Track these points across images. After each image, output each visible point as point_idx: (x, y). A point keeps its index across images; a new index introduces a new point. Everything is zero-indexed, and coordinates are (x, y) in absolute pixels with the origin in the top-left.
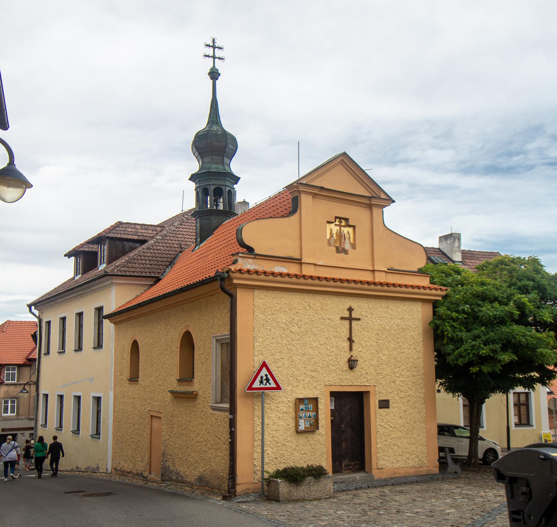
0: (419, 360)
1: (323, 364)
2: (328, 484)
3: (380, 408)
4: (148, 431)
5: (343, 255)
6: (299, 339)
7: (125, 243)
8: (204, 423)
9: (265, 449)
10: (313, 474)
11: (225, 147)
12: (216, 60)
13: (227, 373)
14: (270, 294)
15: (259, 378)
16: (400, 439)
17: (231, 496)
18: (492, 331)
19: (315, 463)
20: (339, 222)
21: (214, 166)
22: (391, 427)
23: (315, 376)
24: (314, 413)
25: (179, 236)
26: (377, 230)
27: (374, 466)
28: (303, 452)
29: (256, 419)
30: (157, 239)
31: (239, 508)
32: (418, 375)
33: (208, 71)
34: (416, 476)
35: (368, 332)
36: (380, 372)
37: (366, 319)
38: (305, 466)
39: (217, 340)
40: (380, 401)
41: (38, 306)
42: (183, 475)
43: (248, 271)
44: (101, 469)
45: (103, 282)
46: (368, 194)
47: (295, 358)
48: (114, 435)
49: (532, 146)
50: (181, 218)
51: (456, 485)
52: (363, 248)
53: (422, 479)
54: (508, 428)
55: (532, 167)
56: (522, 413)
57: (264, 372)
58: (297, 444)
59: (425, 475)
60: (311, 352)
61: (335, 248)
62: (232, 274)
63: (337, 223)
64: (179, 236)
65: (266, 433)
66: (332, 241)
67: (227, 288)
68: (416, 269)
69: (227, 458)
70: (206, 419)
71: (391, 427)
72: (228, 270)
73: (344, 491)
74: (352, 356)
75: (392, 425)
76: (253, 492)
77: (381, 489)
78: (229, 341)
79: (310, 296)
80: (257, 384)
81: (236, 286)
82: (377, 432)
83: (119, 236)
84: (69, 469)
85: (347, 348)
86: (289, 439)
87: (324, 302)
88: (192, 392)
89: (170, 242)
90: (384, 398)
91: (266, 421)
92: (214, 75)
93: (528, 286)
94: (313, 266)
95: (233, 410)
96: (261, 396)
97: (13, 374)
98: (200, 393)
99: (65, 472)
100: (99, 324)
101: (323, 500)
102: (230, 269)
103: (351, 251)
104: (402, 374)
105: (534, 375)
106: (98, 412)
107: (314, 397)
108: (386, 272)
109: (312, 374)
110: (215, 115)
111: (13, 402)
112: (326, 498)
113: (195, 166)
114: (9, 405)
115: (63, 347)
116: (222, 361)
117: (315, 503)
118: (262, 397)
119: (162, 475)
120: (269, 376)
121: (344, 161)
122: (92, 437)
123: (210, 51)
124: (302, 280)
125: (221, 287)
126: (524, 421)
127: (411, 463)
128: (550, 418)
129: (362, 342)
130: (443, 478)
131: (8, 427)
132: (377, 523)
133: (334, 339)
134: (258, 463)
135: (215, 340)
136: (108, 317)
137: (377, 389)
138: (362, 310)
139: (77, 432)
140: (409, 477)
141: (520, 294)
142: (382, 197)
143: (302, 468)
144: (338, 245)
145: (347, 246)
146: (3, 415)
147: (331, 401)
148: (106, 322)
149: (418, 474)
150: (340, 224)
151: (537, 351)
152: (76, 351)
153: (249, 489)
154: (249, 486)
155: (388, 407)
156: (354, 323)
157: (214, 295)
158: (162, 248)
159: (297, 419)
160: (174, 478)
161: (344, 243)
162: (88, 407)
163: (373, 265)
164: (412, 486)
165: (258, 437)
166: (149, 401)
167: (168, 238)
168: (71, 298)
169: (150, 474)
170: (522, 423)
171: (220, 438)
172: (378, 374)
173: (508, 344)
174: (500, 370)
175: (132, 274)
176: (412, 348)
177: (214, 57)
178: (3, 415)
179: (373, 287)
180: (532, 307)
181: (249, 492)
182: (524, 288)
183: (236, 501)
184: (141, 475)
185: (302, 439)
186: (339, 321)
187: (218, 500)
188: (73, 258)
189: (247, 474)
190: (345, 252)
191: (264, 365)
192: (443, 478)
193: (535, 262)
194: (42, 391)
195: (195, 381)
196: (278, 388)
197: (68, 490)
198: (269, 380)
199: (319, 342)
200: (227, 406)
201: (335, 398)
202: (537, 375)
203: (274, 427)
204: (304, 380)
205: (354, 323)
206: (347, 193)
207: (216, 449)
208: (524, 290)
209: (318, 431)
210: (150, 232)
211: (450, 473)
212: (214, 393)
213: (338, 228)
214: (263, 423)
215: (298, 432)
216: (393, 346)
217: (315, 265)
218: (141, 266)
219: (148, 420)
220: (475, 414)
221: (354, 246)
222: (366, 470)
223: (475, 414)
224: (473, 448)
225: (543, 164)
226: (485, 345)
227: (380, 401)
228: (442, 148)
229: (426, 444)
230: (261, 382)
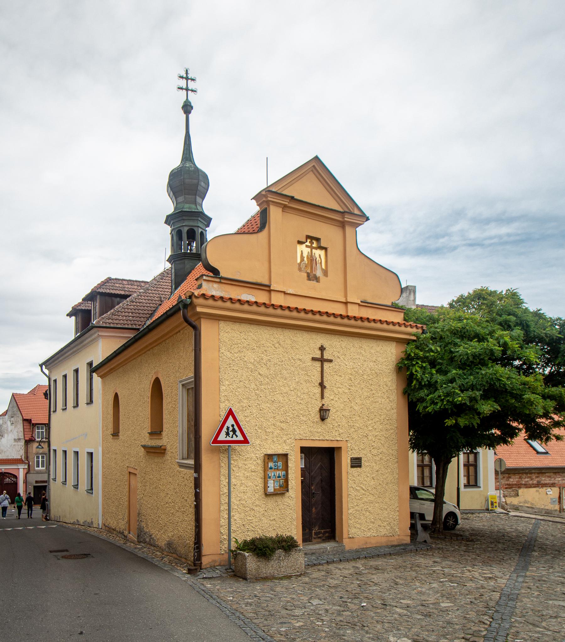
0: (393, 411)
1: (293, 414)
2: (298, 559)
3: (352, 467)
4: (127, 487)
6: (268, 384)
7: (114, 298)
8: (172, 482)
9: (232, 514)
10: (283, 546)
11: (197, 185)
12: (189, 92)
13: (193, 423)
14: (237, 326)
16: (374, 503)
17: (196, 569)
18: (471, 374)
19: (285, 533)
20: (310, 242)
21: (187, 206)
22: (363, 490)
23: (284, 428)
24: (284, 473)
25: (159, 289)
26: (350, 256)
27: (345, 535)
28: (271, 519)
29: (222, 478)
30: (140, 293)
31: (202, 587)
32: (391, 429)
34: (387, 547)
35: (340, 376)
36: (352, 424)
37: (339, 360)
38: (274, 535)
39: (183, 385)
40: (352, 459)
42: (155, 538)
43: (213, 297)
46: (342, 210)
47: (263, 406)
49: (456, 228)
50: (162, 275)
51: (433, 560)
52: (335, 275)
53: (395, 550)
54: (458, 489)
55: (455, 248)
56: (470, 474)
58: (266, 509)
59: (396, 546)
60: (281, 399)
61: (306, 274)
62: (195, 300)
63: (308, 243)
64: (159, 289)
65: (233, 495)
66: (303, 266)
67: (192, 320)
68: (389, 304)
69: (193, 523)
70: (174, 477)
71: (363, 490)
72: (190, 294)
73: (315, 565)
74: (323, 405)
75: (364, 487)
76: (220, 565)
77: (353, 564)
78: (193, 386)
79: (280, 330)
80: (222, 437)
81: (200, 316)
82: (348, 495)
83: (108, 291)
85: (318, 395)
86: (257, 502)
87: (295, 339)
88: (161, 446)
89: (152, 295)
90: (356, 456)
91: (233, 481)
92: (187, 108)
93: (510, 321)
94: (283, 294)
95: (197, 468)
96: (227, 450)
98: (168, 448)
99: (70, 525)
101: (293, 579)
102: (193, 293)
104: (375, 427)
105: (495, 433)
107: (283, 453)
108: (359, 305)
109: (282, 425)
110: (188, 152)
111: (43, 457)
112: (297, 575)
113: (169, 207)
114: (40, 460)
116: (188, 409)
117: (285, 582)
118: (228, 452)
119: (138, 536)
120: (236, 427)
121: (316, 168)
123: (183, 83)
124: (271, 311)
125: (185, 317)
126: (472, 483)
127: (383, 532)
128: (496, 479)
129: (335, 388)
130: (417, 550)
131: (40, 480)
132: (366, 628)
133: (304, 383)
134: (224, 530)
135: (181, 386)
137: (349, 445)
138: (335, 349)
139: (76, 487)
140: (380, 547)
141: (502, 330)
142: (355, 213)
143: (271, 539)
144: (309, 271)
145: (319, 273)
146: (36, 469)
147: (301, 458)
148: (95, 375)
149: (389, 544)
150: (311, 245)
151: (523, 399)
152: (74, 407)
153: (214, 561)
154: (216, 558)
155: (360, 466)
156: (326, 365)
158: (144, 301)
159: (266, 478)
160: (148, 540)
161: (316, 269)
163: (346, 296)
164: (386, 560)
165: (225, 499)
167: (150, 291)
169: (129, 533)
170: (471, 484)
172: (351, 427)
173: (493, 391)
174: (477, 423)
175: (115, 326)
176: (385, 397)
177: (187, 90)
178: (36, 469)
179: (346, 321)
180: (517, 346)
181: (216, 565)
182: (506, 324)
183: (201, 576)
185: (271, 502)
186: (310, 363)
187: (181, 573)
188: (73, 318)
189: (214, 547)
190: (317, 279)
191: (230, 413)
192: (417, 550)
193: (513, 296)
194: (53, 447)
195: (164, 433)
196: (246, 441)
197: (56, 548)
198: (236, 431)
199: (289, 387)
200: (191, 462)
201: (305, 455)
202: (498, 433)
203: (242, 488)
204: (273, 433)
205: (326, 365)
206: (319, 206)
207: (183, 512)
208: (506, 326)
209: (287, 494)
210: (136, 287)
211: (420, 543)
212: (181, 447)
213: (309, 250)
214: (229, 483)
215: (267, 495)
216: (365, 394)
217: (285, 293)
218: (124, 318)
219: (127, 477)
220: (441, 475)
221: (325, 273)
222: (337, 539)
223: (441, 475)
224: (438, 512)
225: (465, 245)
226: (462, 391)
227: (352, 459)
228: (381, 232)
229: (398, 509)
230: (227, 434)
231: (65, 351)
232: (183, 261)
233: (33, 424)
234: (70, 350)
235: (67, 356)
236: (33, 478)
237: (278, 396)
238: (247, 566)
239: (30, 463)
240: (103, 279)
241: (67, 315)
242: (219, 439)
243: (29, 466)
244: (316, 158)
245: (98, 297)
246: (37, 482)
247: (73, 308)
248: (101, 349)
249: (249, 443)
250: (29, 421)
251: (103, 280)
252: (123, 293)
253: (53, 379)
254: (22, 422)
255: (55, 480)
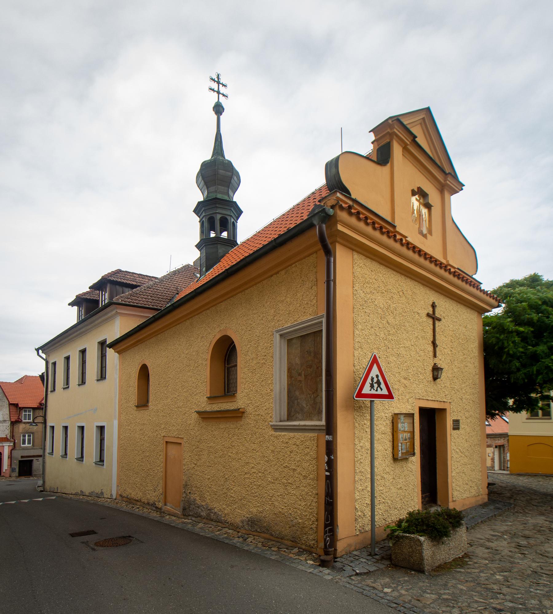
4: (162, 458)
11: (231, 178)
15: (369, 381)
27: (450, 500)
33: (213, 105)
40: (454, 421)
41: (44, 350)
42: (220, 513)
44: (105, 494)
45: (106, 314)
48: (119, 462)
57: (375, 371)
74: (435, 364)
80: (367, 390)
84: (74, 493)
85: (431, 354)
88: (239, 409)
92: (218, 109)
95: (330, 428)
97: (29, 415)
98: (250, 409)
99: (71, 496)
100: (102, 357)
106: (102, 440)
111: (29, 436)
114: (27, 438)
115: (68, 383)
122: (96, 464)
123: (215, 86)
136: (111, 346)
139: (81, 458)
146: (22, 445)
148: (110, 352)
153: (349, 545)
157: (278, 273)
160: (204, 514)
162: (91, 437)
166: (163, 426)
168: (75, 337)
169: (165, 505)
171: (294, 470)
177: (218, 93)
178: (22, 445)
184: (153, 505)
186: (425, 319)
187: (308, 564)
189: (351, 522)
194: (49, 424)
196: (390, 396)
199: (410, 341)
205: (437, 323)
212: (278, 407)
222: (439, 503)
230: (372, 386)
231: (70, 332)
232: (216, 245)
233: (20, 408)
234: (77, 331)
235: (72, 338)
236: (18, 454)
237: (402, 349)
238: (424, 555)
239: (16, 441)
240: (114, 269)
241: (69, 304)
242: (364, 392)
243: (14, 443)
244: (428, 110)
245: (109, 285)
246: (22, 457)
247: (77, 296)
248: (117, 327)
249: (393, 398)
250: (16, 405)
251: (114, 270)
252: (134, 283)
253: (51, 361)
254: (8, 406)
255: (52, 453)
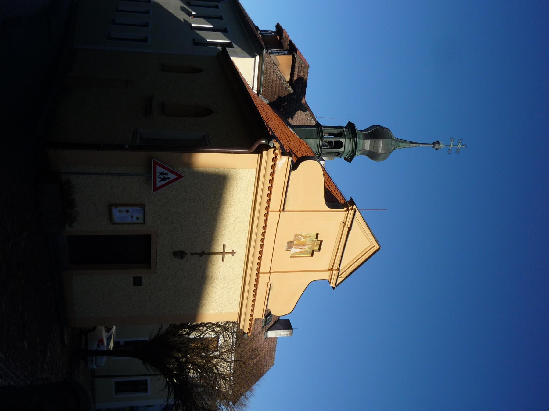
5: (285, 246)
15: (165, 171)
57: (172, 176)
61: (292, 240)
62: (272, 150)
103: (289, 253)
120: (168, 181)
144: (295, 242)
161: (297, 248)
191: (179, 177)
196: (156, 189)
230: (162, 174)
241: (278, 24)
